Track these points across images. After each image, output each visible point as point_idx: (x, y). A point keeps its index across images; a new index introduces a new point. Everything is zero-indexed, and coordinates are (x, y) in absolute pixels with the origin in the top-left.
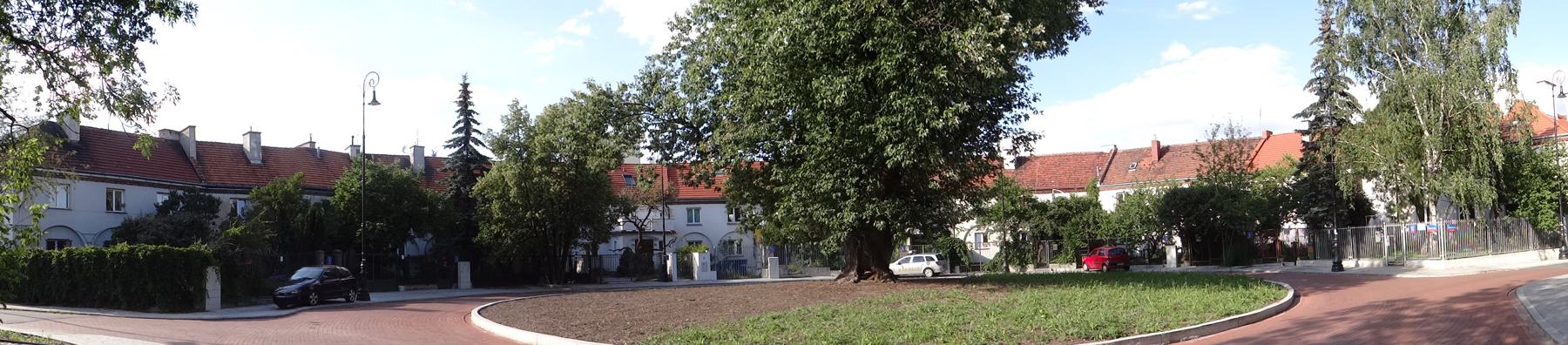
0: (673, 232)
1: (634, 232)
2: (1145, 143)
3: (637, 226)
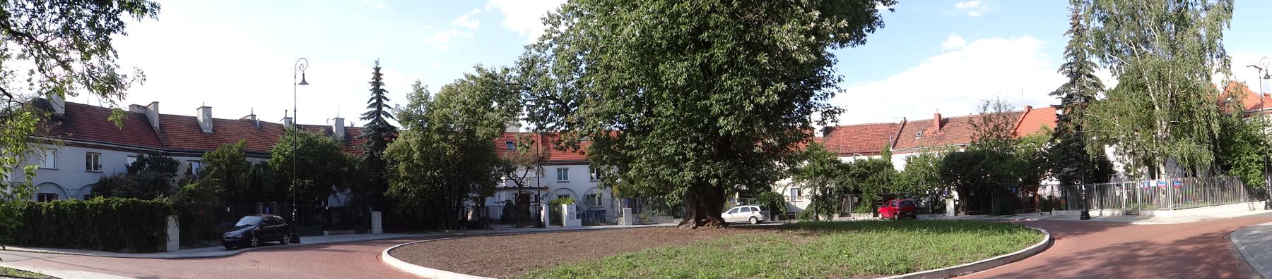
0: (546, 188)
1: (514, 188)
3: (517, 183)
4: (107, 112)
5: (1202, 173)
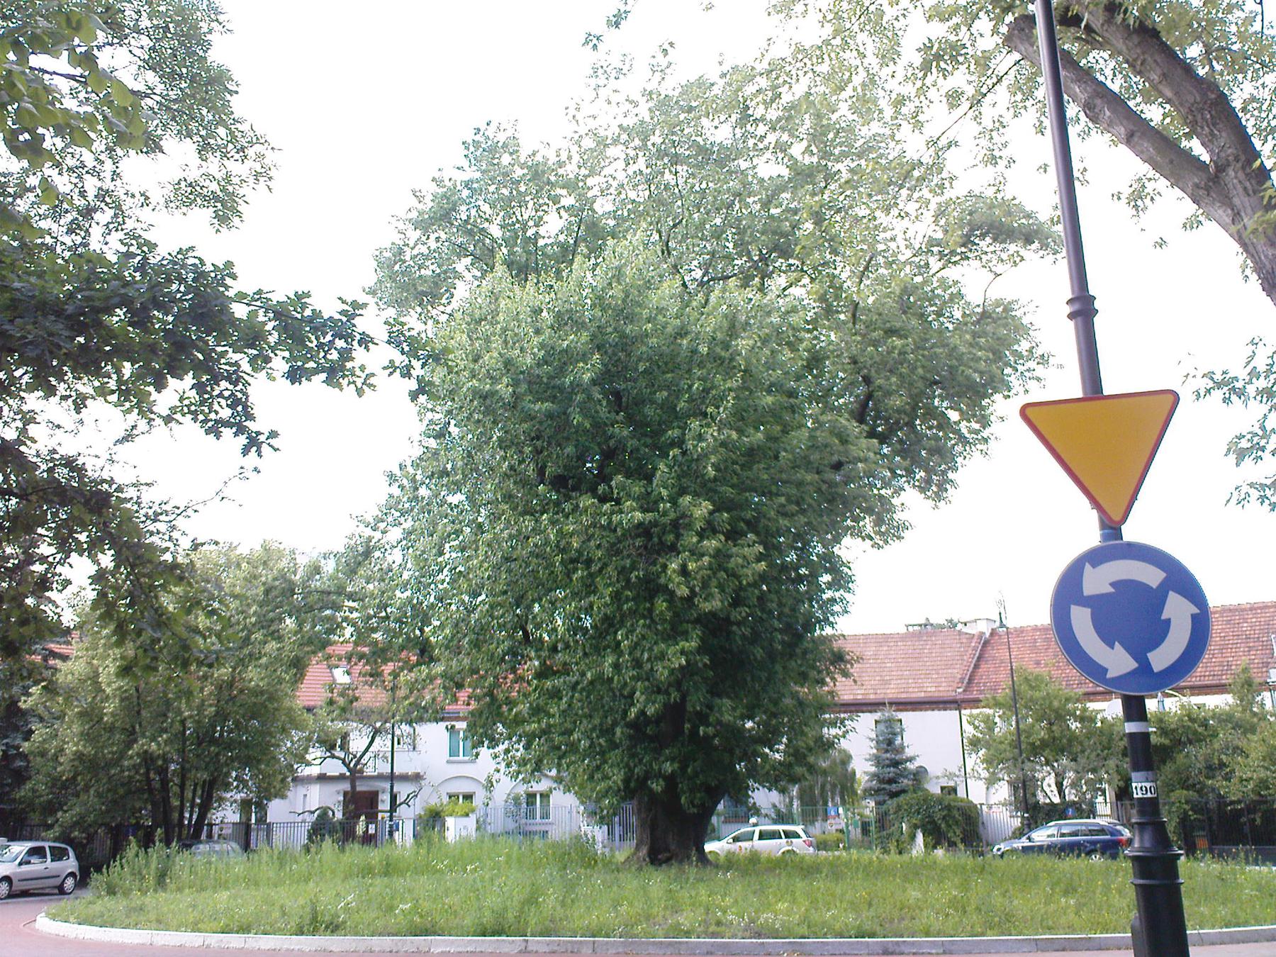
0: (417, 777)
1: (342, 777)
2: (942, 621)
3: (347, 766)
4: (971, 708)
5: (689, 343)
